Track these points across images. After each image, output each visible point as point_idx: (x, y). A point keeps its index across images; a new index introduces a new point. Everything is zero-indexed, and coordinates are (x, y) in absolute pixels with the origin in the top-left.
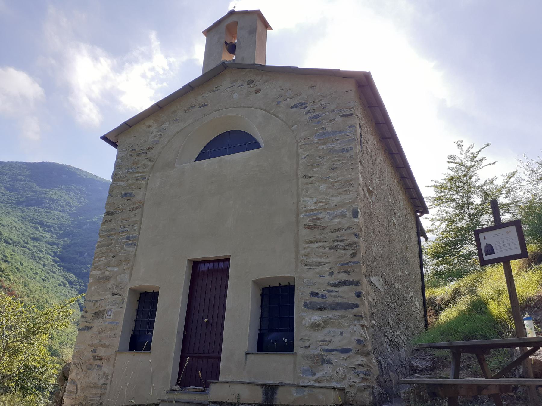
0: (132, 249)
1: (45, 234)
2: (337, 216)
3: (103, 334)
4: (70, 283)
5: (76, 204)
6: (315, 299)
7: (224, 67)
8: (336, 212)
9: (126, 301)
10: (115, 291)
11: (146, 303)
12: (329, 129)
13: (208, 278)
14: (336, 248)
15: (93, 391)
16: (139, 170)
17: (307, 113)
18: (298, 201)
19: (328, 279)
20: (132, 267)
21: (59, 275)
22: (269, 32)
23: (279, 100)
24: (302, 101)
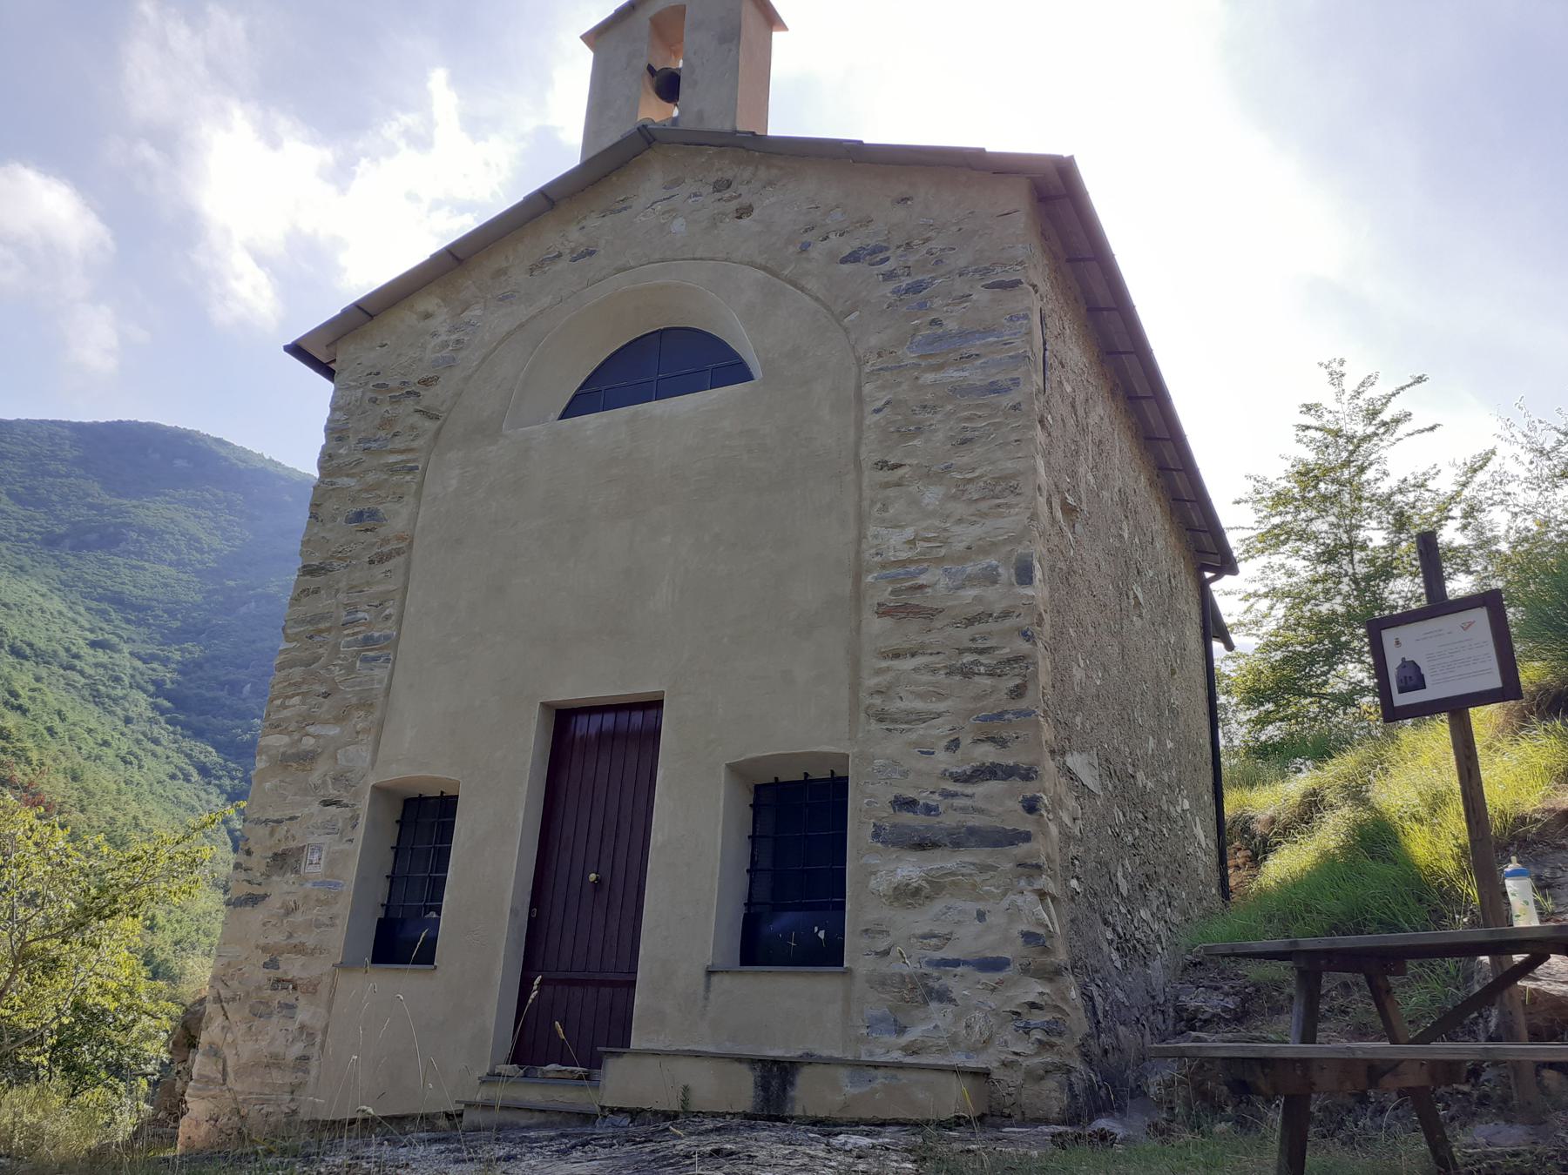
0: (380, 673)
2: (971, 580)
3: (298, 918)
4: (204, 771)
5: (216, 544)
6: (907, 818)
7: (646, 139)
8: (970, 568)
9: (362, 822)
10: (332, 793)
12: (952, 325)
13: (598, 755)
14: (967, 673)
15: (277, 1077)
16: (398, 443)
17: (889, 276)
18: (861, 537)
19: (943, 760)
20: (381, 725)
21: (172, 748)
23: (807, 238)
24: (872, 242)
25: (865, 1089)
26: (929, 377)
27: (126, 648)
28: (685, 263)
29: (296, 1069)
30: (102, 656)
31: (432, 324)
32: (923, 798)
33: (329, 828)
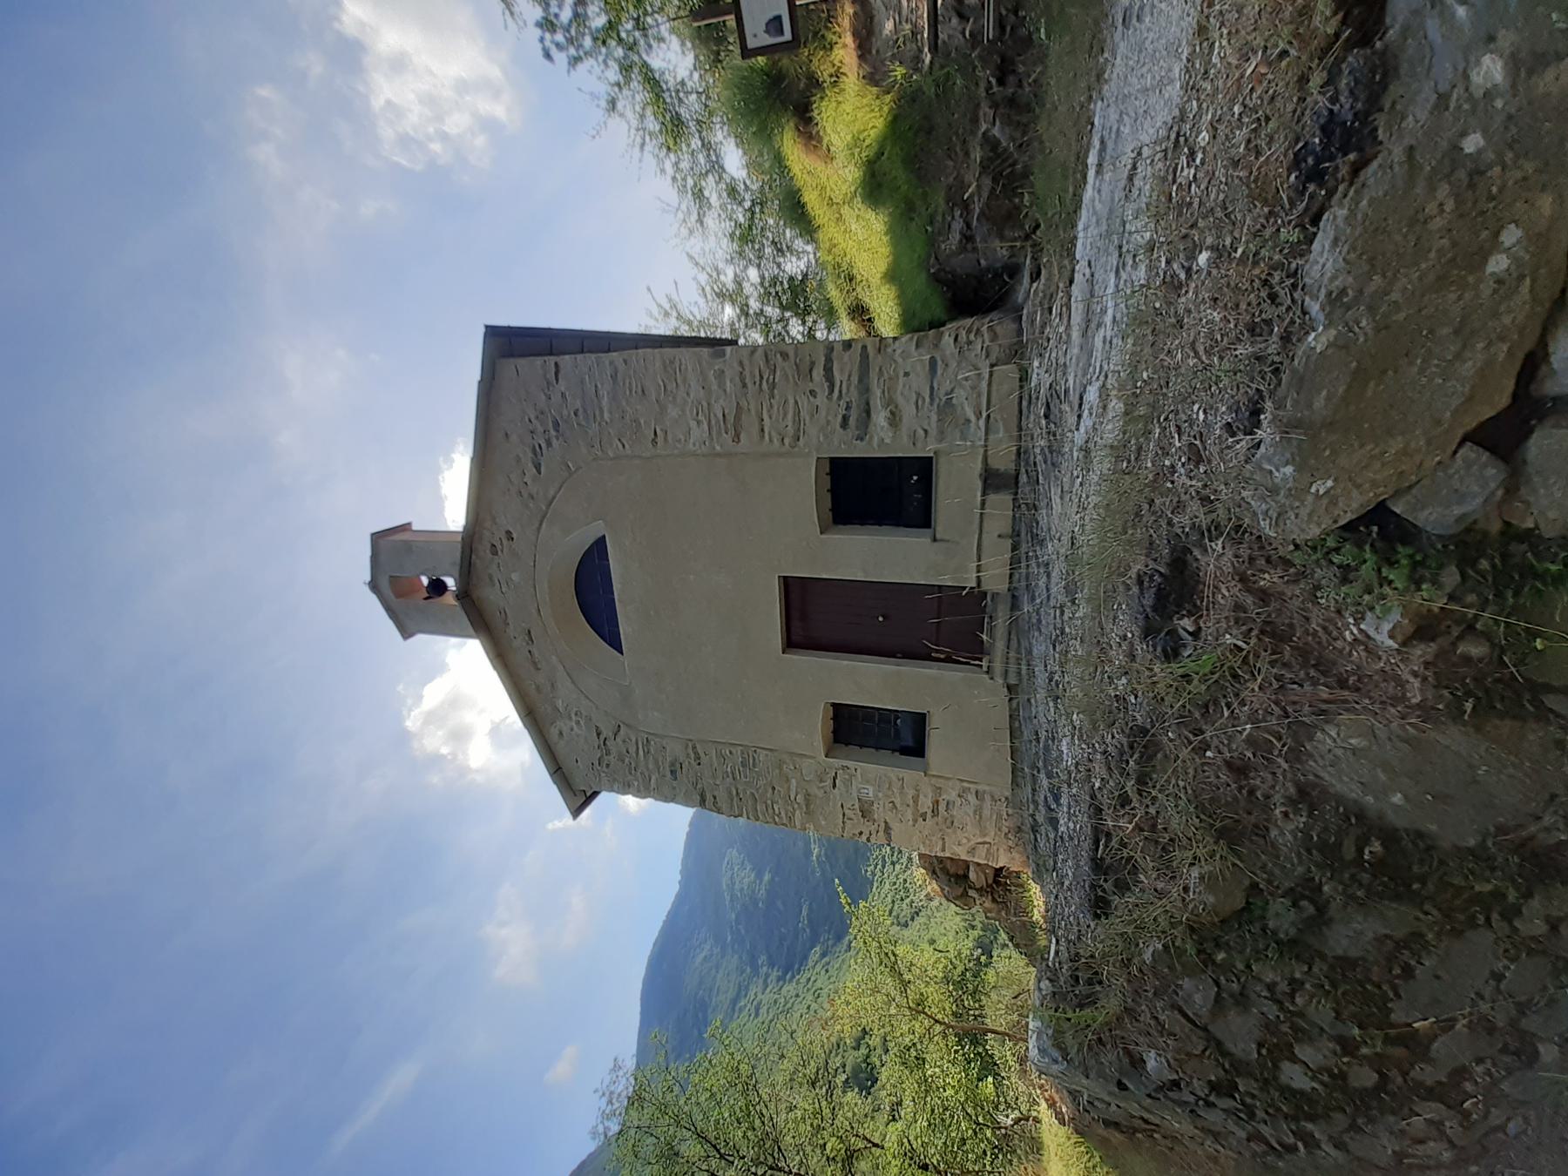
0: (762, 755)
1: (751, 994)
2: (721, 385)
3: (898, 801)
4: (824, 955)
5: (707, 947)
6: (852, 421)
7: (464, 595)
8: (715, 387)
9: (845, 763)
10: (829, 782)
11: (853, 728)
12: (578, 404)
13: (815, 617)
14: (773, 386)
15: (986, 812)
16: (632, 750)
17: (549, 444)
18: (694, 454)
19: (821, 400)
20: (792, 754)
21: (814, 969)
22: (415, 527)
23: (525, 495)
24: (530, 455)
25: (1001, 424)
26: (606, 415)
27: (760, 996)
28: (538, 580)
29: (983, 799)
30: (763, 1010)
31: (565, 730)
32: (842, 411)
33: (848, 783)
